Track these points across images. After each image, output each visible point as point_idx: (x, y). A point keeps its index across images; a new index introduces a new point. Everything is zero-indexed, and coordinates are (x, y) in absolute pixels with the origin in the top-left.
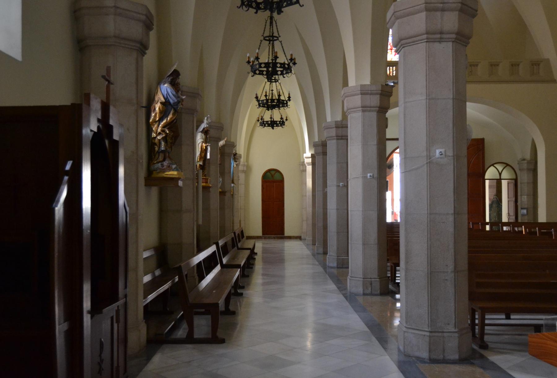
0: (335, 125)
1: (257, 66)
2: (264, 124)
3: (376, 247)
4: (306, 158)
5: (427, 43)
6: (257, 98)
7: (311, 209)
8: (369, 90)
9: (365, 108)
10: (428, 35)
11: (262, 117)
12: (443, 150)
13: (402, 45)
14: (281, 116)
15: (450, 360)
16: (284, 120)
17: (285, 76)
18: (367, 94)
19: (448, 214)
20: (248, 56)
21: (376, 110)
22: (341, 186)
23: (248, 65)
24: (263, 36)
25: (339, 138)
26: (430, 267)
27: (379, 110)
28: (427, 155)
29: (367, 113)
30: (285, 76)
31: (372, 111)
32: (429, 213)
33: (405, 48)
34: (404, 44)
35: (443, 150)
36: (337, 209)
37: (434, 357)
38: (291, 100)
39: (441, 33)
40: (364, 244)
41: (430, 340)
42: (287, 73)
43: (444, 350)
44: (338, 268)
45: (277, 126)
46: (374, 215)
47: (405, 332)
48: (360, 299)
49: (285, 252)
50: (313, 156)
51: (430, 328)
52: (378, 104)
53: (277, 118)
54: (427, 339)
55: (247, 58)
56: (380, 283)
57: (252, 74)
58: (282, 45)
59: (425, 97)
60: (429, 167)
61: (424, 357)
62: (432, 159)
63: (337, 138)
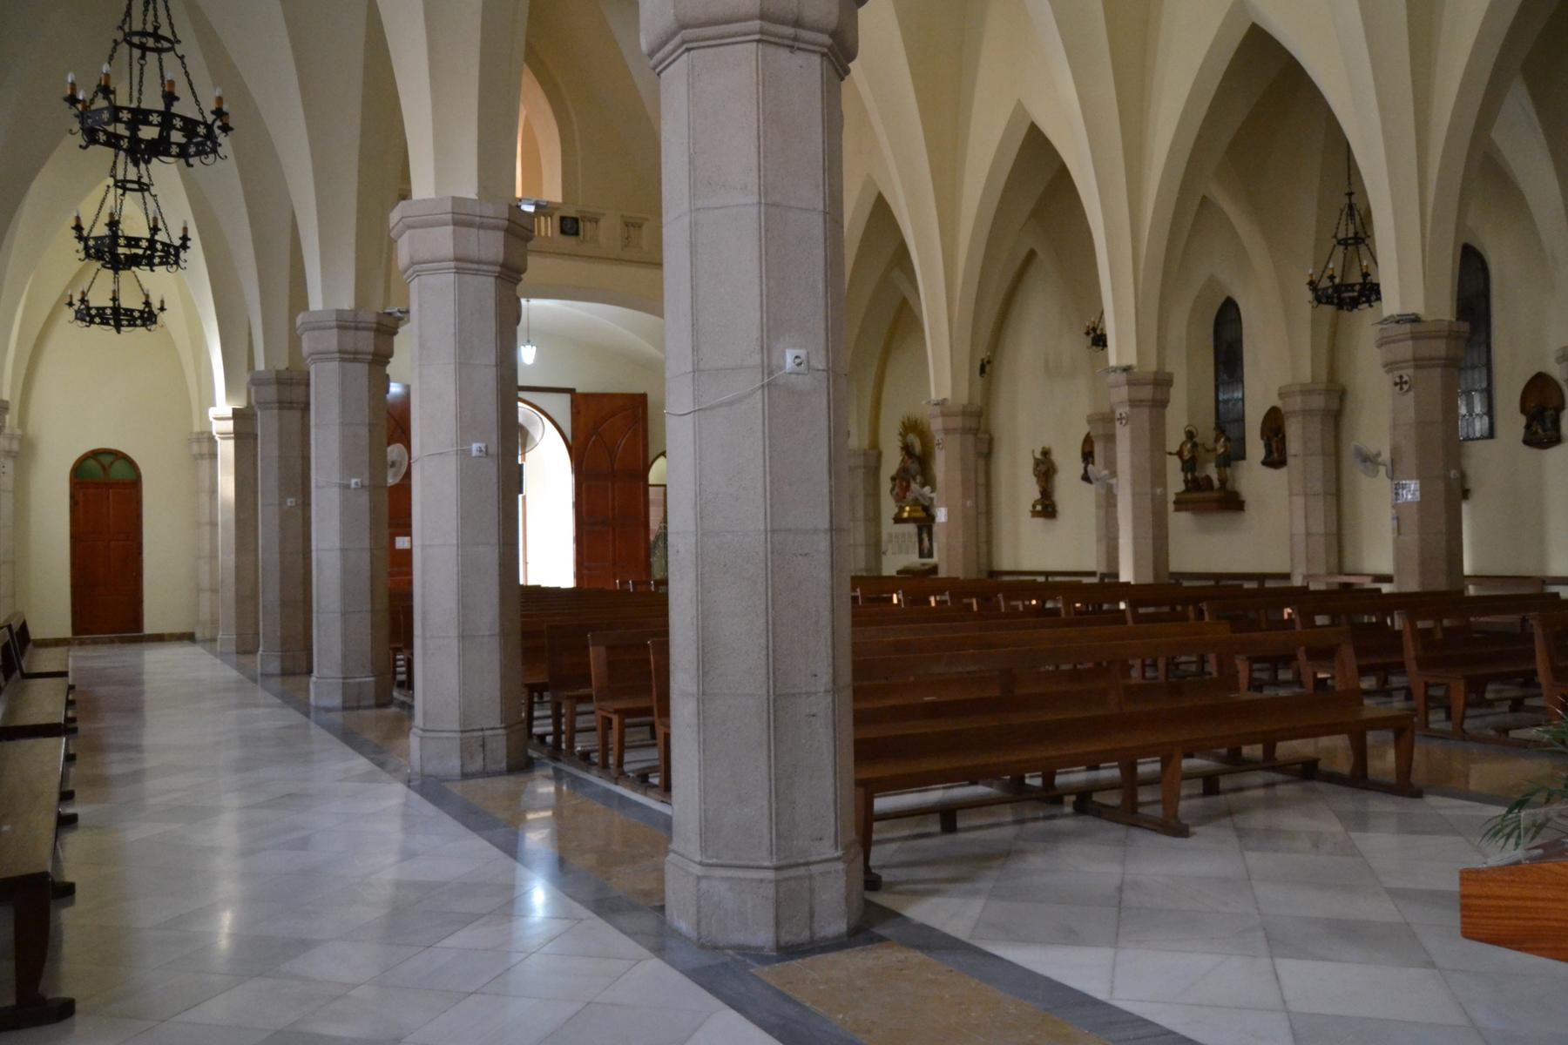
0: (337, 320)
1: (106, 116)
2: (88, 315)
3: (495, 643)
4: (216, 419)
5: (760, 46)
6: (78, 227)
7: (233, 556)
8: (476, 216)
9: (463, 264)
10: (763, 23)
11: (84, 294)
12: (802, 352)
13: (684, 42)
14: (147, 296)
15: (826, 939)
16: (156, 311)
17: (191, 160)
18: (470, 225)
19: (816, 531)
20: (70, 80)
21: (495, 272)
22: (353, 486)
23: (71, 108)
24: (121, 28)
25: (346, 356)
26: (774, 682)
27: (500, 273)
28: (763, 362)
29: (468, 278)
30: (191, 160)
31: (486, 273)
32: (769, 529)
33: (692, 52)
34: (692, 41)
35: (802, 352)
36: (343, 550)
37: (787, 938)
38: (189, 247)
39: (797, 23)
40: (463, 637)
41: (777, 892)
42: (198, 153)
43: (812, 916)
44: (345, 708)
45: (132, 323)
46: (490, 555)
47: (699, 878)
48: (456, 788)
49: (145, 677)
50: (237, 415)
51: (775, 857)
52: (501, 257)
53: (131, 301)
54: (770, 892)
55: (69, 86)
56: (507, 740)
57: (80, 139)
58: (185, 68)
59: (755, 199)
60: (769, 398)
61: (762, 945)
62: (776, 375)
63: (342, 356)
